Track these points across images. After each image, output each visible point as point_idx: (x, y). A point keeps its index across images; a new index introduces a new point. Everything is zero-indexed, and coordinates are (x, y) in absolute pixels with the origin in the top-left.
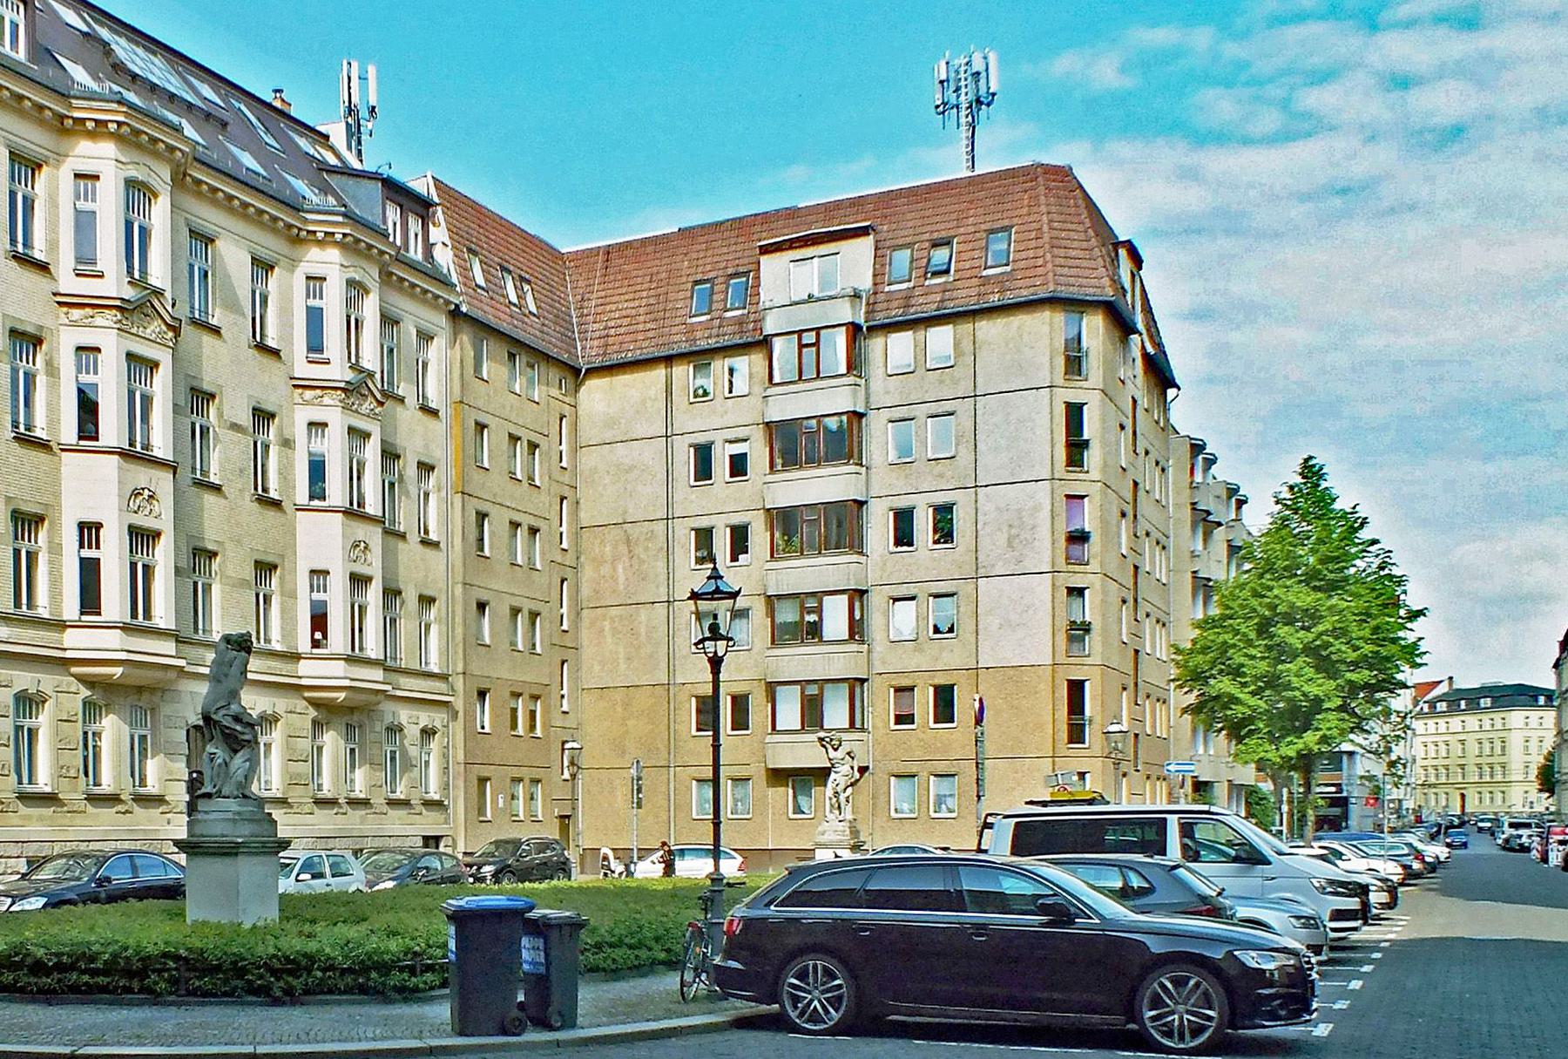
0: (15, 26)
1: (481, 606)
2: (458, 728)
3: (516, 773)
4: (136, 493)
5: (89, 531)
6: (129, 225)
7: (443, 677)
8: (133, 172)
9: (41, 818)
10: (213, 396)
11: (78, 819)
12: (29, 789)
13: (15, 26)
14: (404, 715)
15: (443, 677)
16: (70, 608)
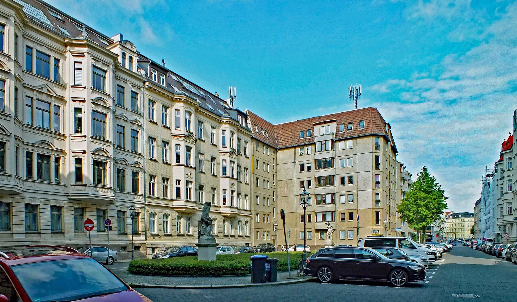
0: (163, 80)
1: (257, 197)
2: (253, 221)
4: (188, 174)
5: (178, 181)
6: (186, 120)
7: (250, 211)
8: (187, 109)
9: (168, 240)
10: (203, 154)
11: (176, 239)
12: (166, 233)
13: (163, 80)
14: (242, 219)
15: (250, 211)
16: (174, 197)
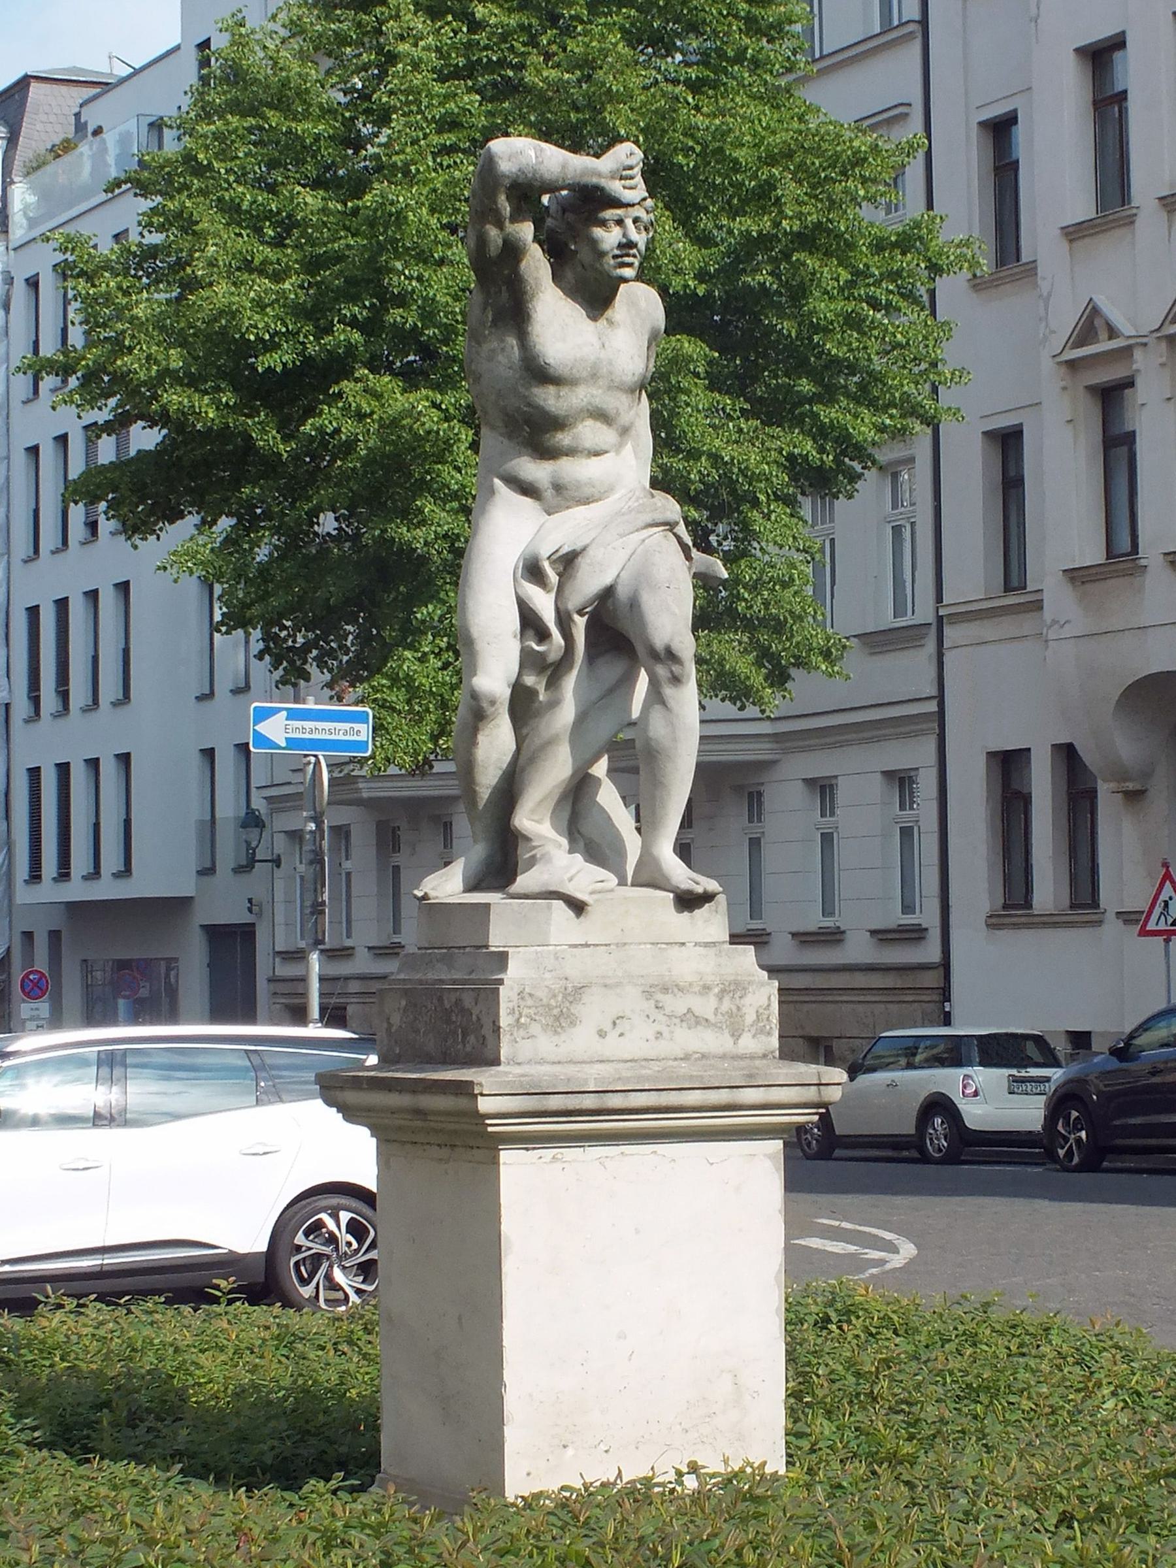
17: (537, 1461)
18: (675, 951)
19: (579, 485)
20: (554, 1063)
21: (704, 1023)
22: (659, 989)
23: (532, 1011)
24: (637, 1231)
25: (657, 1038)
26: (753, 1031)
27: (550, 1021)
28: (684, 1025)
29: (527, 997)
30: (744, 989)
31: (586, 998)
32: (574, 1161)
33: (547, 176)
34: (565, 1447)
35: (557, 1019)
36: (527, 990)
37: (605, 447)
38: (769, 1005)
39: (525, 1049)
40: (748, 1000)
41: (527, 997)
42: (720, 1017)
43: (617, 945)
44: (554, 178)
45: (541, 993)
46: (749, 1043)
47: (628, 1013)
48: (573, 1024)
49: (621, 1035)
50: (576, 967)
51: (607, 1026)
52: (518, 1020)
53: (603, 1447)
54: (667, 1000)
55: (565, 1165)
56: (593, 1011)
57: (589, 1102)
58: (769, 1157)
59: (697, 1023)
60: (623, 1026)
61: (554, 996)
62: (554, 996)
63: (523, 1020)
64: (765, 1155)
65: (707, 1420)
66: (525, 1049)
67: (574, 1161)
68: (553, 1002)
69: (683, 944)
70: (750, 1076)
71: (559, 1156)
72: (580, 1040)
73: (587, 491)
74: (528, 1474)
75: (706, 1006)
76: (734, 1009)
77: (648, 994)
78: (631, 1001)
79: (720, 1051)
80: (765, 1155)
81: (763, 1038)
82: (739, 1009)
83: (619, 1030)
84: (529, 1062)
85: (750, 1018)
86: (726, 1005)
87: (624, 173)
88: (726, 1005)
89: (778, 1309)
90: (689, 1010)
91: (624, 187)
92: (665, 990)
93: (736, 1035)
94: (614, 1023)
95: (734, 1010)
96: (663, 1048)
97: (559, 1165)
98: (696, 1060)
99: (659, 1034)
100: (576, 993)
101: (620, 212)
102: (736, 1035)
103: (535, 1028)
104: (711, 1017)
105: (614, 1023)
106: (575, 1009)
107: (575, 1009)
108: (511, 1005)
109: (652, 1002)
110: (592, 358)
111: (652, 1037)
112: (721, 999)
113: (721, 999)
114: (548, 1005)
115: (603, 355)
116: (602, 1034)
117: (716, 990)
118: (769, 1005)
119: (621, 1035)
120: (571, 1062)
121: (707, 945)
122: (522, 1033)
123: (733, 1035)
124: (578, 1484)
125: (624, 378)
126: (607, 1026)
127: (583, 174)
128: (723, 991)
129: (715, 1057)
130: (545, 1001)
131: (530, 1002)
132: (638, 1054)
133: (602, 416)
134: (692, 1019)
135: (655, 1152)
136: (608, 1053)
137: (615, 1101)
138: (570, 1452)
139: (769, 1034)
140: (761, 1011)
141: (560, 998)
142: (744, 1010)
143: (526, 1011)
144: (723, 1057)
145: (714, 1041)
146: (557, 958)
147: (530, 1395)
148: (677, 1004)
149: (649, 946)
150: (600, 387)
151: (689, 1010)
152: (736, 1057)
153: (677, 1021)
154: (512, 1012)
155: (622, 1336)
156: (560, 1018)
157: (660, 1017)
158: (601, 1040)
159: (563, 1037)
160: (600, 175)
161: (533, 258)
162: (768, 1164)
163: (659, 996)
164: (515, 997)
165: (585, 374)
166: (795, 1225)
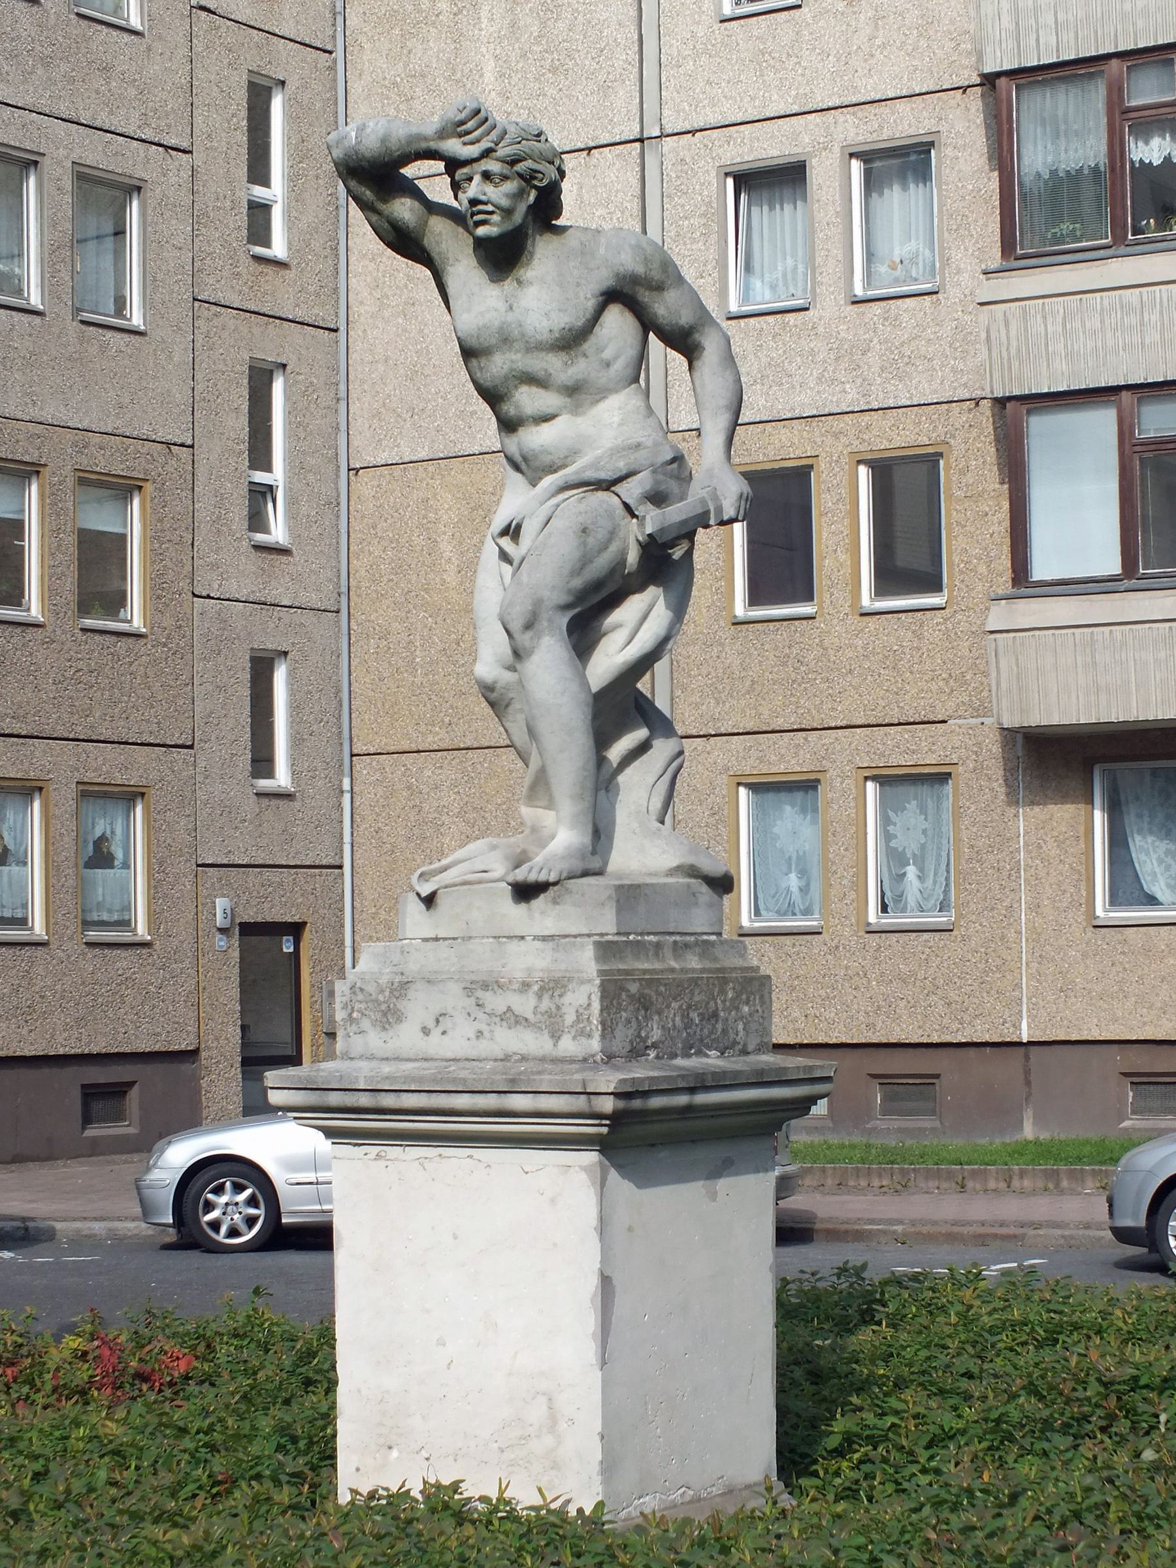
3: (106, 766)
17: (369, 1461)
18: (513, 946)
19: (545, 451)
20: (383, 1059)
21: (523, 1022)
22: (478, 986)
23: (363, 1006)
24: (455, 1237)
25: (478, 1037)
26: (573, 1031)
27: (379, 1016)
28: (504, 1024)
29: (358, 991)
30: (564, 986)
31: (411, 994)
32: (396, 1159)
33: (368, 154)
34: (390, 1448)
35: (385, 1014)
36: (358, 985)
37: (550, 411)
38: (589, 1005)
39: (357, 1044)
40: (568, 998)
41: (358, 991)
42: (539, 1016)
43: (463, 938)
44: (376, 155)
45: (371, 988)
46: (568, 1046)
47: (450, 1011)
48: (399, 1020)
49: (444, 1033)
50: (418, 961)
51: (431, 1024)
52: (350, 1015)
53: (425, 1454)
54: (487, 997)
55: (388, 1163)
56: (419, 1007)
57: (364, 1100)
58: (584, 1169)
59: (517, 1022)
60: (446, 1023)
61: (382, 991)
62: (382, 991)
63: (355, 1015)
64: (580, 1167)
65: (523, 1442)
66: (357, 1044)
67: (396, 1159)
68: (381, 998)
69: (523, 938)
70: (513, 1081)
71: (383, 1154)
72: (406, 1038)
73: (547, 459)
74: (358, 1470)
75: (525, 1005)
76: (553, 1007)
77: (469, 991)
78: (453, 998)
79: (540, 1053)
80: (580, 1167)
81: (583, 1040)
82: (558, 1008)
83: (441, 1029)
84: (361, 1057)
85: (570, 1018)
86: (546, 1003)
87: (459, 129)
88: (546, 1003)
89: (594, 1334)
90: (509, 1009)
91: (465, 144)
92: (485, 986)
93: (556, 1036)
94: (438, 1021)
95: (554, 1009)
96: (483, 1048)
97: (382, 1163)
98: (516, 1061)
99: (480, 1034)
100: (401, 988)
101: (465, 170)
102: (556, 1036)
103: (366, 1024)
104: (530, 1016)
105: (438, 1021)
106: (402, 1005)
107: (402, 1005)
108: (344, 999)
109: (473, 1000)
110: (497, 323)
111: (473, 1036)
112: (540, 997)
113: (540, 997)
114: (377, 1001)
115: (510, 317)
116: (426, 1031)
117: (536, 988)
118: (589, 1005)
119: (444, 1033)
120: (467, 1059)
121: (544, 939)
122: (354, 1028)
123: (553, 1036)
124: (494, 1495)
125: (539, 337)
126: (431, 1024)
127: (409, 143)
128: (542, 989)
129: (535, 1059)
130: (374, 997)
131: (360, 997)
132: (460, 1054)
133: (531, 379)
134: (511, 1018)
135: (470, 1157)
136: (432, 1052)
137: (388, 1101)
138: (395, 1454)
139: (589, 1036)
140: (581, 1011)
141: (387, 994)
142: (564, 1010)
143: (357, 1006)
144: (543, 1059)
145: (533, 1043)
146: (402, 952)
147: (359, 1391)
148: (497, 1002)
149: (491, 940)
150: (517, 351)
151: (509, 1009)
152: (555, 1060)
153: (498, 1019)
154: (345, 1007)
155: (441, 1343)
156: (389, 1016)
157: (481, 1016)
158: (426, 1038)
159: (391, 1033)
160: (426, 139)
161: (432, 233)
162: (583, 1176)
163: (480, 993)
164: (347, 992)
165: (493, 341)
166: (776, 1257)
